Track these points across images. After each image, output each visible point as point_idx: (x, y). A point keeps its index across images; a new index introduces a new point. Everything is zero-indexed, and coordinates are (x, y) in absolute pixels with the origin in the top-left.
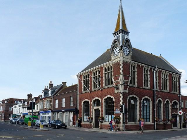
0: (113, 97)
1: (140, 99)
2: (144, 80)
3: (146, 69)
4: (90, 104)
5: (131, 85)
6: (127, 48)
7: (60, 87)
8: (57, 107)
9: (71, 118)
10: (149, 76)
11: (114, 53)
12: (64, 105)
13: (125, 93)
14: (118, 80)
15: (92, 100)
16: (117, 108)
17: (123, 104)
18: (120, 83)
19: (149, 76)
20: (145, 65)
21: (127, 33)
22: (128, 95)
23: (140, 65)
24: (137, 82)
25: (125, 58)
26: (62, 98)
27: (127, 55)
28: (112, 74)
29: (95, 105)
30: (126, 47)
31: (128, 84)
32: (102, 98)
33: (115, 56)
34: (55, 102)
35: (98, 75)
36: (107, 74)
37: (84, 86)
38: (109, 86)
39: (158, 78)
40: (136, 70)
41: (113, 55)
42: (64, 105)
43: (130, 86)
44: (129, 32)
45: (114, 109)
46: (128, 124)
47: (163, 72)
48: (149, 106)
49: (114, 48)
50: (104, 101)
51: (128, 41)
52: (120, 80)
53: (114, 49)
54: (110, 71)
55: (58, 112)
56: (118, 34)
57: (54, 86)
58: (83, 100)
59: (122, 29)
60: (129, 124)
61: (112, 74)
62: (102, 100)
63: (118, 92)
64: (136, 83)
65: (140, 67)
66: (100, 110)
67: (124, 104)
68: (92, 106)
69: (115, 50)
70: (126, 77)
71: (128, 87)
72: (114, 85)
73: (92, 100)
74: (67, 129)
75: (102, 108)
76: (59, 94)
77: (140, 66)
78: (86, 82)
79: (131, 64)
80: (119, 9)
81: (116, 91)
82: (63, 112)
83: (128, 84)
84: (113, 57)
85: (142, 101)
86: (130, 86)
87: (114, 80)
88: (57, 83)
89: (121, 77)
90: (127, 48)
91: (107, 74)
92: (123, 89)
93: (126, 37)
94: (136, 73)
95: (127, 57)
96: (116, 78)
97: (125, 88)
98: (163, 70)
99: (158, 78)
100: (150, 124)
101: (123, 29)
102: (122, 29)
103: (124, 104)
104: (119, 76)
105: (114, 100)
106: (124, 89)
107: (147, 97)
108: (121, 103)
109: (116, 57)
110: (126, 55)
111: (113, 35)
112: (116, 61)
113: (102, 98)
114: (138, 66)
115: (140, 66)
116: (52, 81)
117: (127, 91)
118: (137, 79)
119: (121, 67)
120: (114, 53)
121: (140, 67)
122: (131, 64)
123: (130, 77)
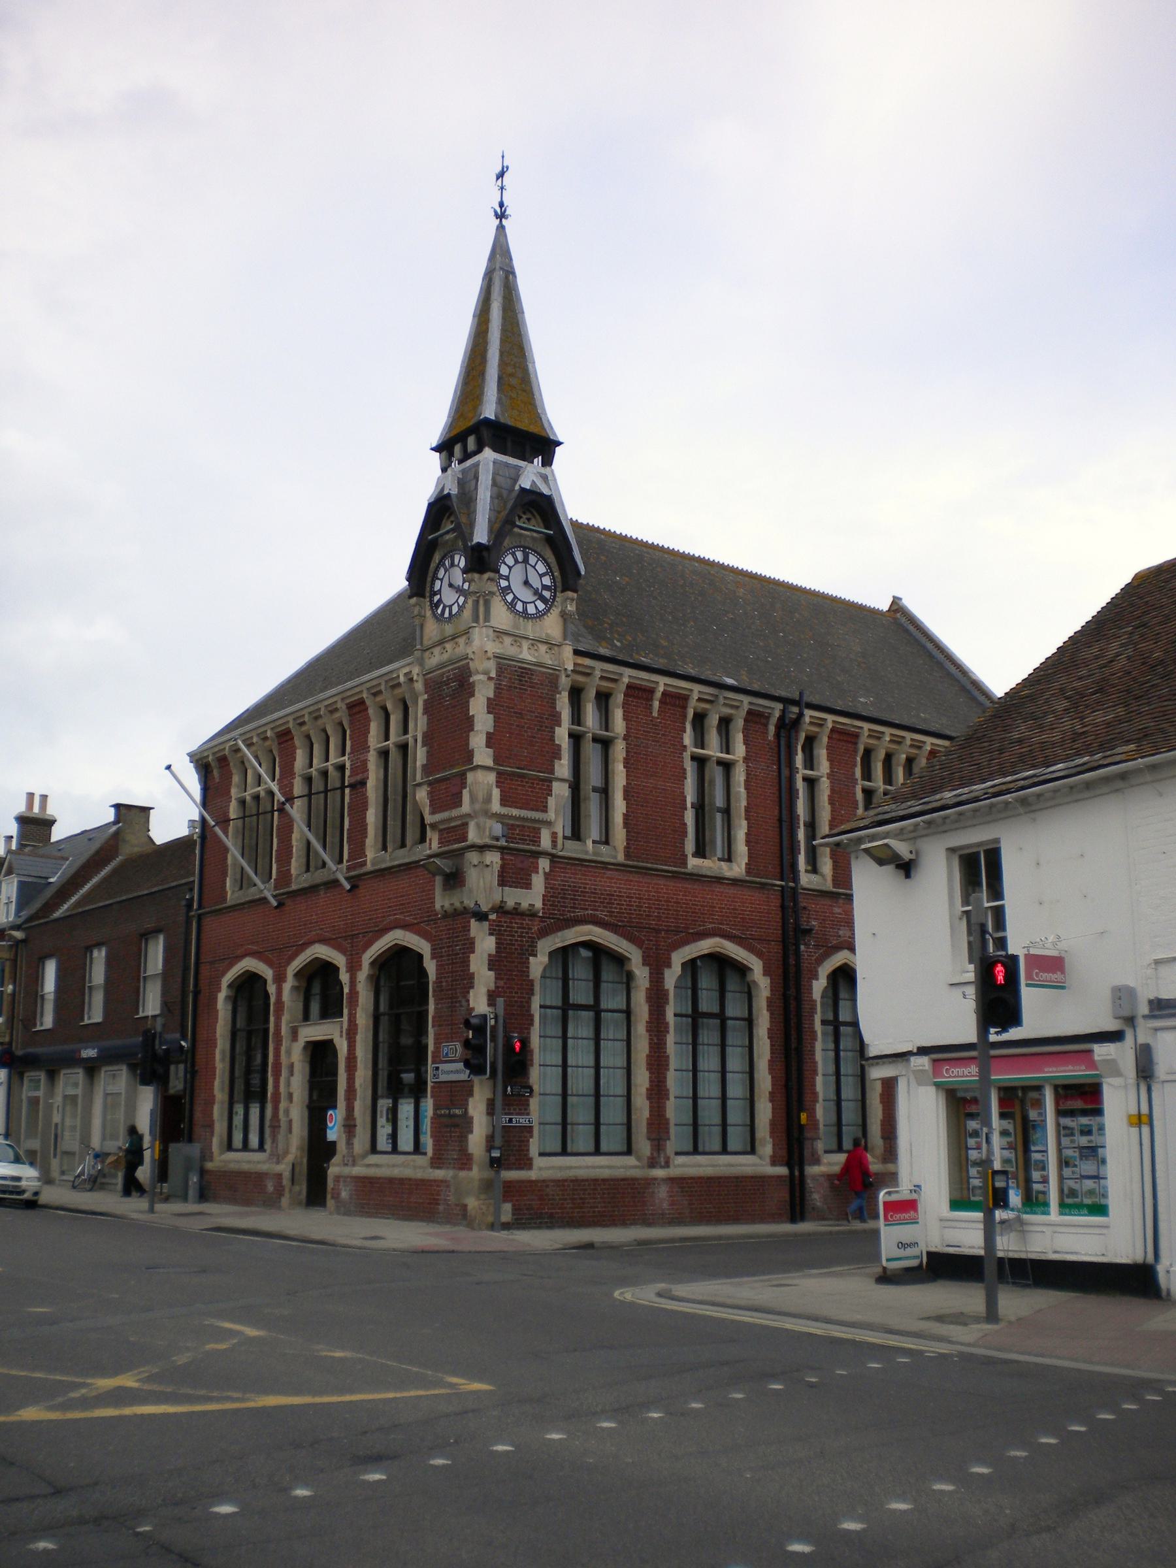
0: (423, 946)
1: (657, 964)
2: (700, 808)
3: (713, 720)
4: (273, 1000)
5: (572, 849)
6: (532, 559)
7: (96, 846)
8: (47, 1021)
9: (144, 1124)
10: (740, 775)
11: (436, 598)
12: (95, 1014)
13: (516, 912)
14: (455, 813)
15: (368, 956)
16: (450, 1039)
17: (491, 1002)
18: (473, 836)
19: (740, 775)
20: (697, 690)
21: (542, 446)
22: (544, 933)
23: (651, 691)
24: (626, 824)
25: (517, 638)
26: (89, 949)
27: (531, 609)
28: (420, 755)
29: (315, 1008)
30: (520, 556)
31: (536, 840)
32: (353, 948)
33: (439, 619)
34: (37, 979)
35: (334, 759)
36: (394, 755)
37: (308, 843)
38: (403, 857)
39: (824, 787)
40: (619, 724)
41: (429, 613)
42: (95, 1014)
43: (553, 858)
44: (561, 440)
45: (431, 1048)
46: (533, 1175)
47: (898, 741)
48: (750, 1021)
49: (437, 557)
50: (370, 977)
51: (542, 506)
52: (466, 807)
53: (433, 565)
54: (410, 736)
55: (53, 1068)
56: (466, 456)
57: (58, 833)
58: (231, 965)
59: (497, 423)
60: (546, 1175)
61: (420, 755)
62: (353, 967)
63: (457, 905)
64: (619, 835)
65: (656, 704)
66: (342, 1047)
67: (500, 1001)
68: (285, 1019)
69: (442, 571)
70: (523, 784)
71: (544, 864)
72: (435, 845)
73: (368, 956)
74: (45, 1206)
75: (353, 1036)
76: (78, 904)
77: (658, 695)
78: (334, 799)
79: (564, 682)
80: (489, 276)
81: (442, 901)
82: (91, 1069)
83: (545, 842)
84: (432, 630)
85: (672, 976)
86: (553, 858)
87: (433, 813)
88: (79, 814)
89: (483, 783)
90: (532, 559)
91: (394, 755)
92: (492, 877)
93: (530, 475)
94: (619, 750)
95: (529, 629)
96: (447, 793)
97: (514, 874)
98: (866, 726)
99: (824, 787)
100: (749, 1171)
101: (506, 420)
102: (497, 423)
103: (500, 1001)
104: (463, 775)
105: (430, 966)
106: (503, 882)
107: (717, 940)
108: (479, 1003)
109: (449, 629)
110: (525, 614)
111: (435, 460)
112: (445, 656)
113: (353, 948)
114: (634, 690)
115: (658, 695)
116: (44, 798)
117: (533, 896)
118: (626, 797)
119: (478, 707)
120: (436, 598)
121: (656, 704)
122: (564, 682)
123: (556, 786)
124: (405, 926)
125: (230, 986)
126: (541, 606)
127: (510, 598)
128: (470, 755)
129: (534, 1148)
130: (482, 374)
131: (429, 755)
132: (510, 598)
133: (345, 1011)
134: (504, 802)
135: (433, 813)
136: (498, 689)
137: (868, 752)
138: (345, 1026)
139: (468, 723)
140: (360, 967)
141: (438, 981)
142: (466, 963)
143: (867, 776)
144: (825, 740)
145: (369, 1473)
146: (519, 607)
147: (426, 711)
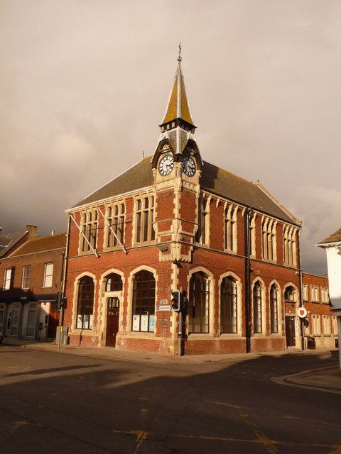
93: (189, 135)
105: (156, 277)
117: (188, 258)
119: (176, 201)
133: (123, 289)
134: (183, 229)
141: (159, 282)
142: (170, 276)
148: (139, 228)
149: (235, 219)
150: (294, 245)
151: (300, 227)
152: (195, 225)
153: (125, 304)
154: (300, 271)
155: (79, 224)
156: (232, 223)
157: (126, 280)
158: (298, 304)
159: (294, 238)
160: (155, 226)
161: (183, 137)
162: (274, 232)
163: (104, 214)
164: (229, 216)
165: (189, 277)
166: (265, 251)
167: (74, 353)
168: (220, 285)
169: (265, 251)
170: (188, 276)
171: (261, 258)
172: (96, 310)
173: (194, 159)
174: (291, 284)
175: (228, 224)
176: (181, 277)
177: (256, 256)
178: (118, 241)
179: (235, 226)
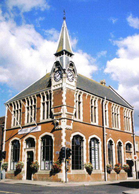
1: (87, 139)
4: (21, 144)
15: (40, 137)
27: (71, 80)
30: (69, 72)
64: (82, 117)
65: (86, 97)
87: (55, 112)
93: (70, 59)
105: (53, 138)
117: (71, 127)
119: (64, 95)
121: (86, 97)
124: (96, 135)
125: (11, 142)
126: (72, 80)
127: (68, 78)
128: (62, 103)
129: (130, 159)
130: (63, 41)
131: (54, 103)
132: (68, 78)
133: (36, 146)
134: (68, 111)
135: (55, 112)
136: (67, 93)
137: (92, 100)
138: (36, 148)
139: (62, 98)
140: (39, 139)
141: (55, 141)
142: (61, 137)
143: (92, 104)
144: (82, 96)
145: (126, 191)
146: (69, 80)
147: (53, 96)
148: (44, 111)
149: (97, 106)
150: (130, 119)
151: (133, 109)
152: (74, 109)
153: (107, 163)
154: (133, 134)
155: (12, 111)
156: (95, 108)
157: (37, 141)
158: (133, 153)
159: (130, 116)
160: (52, 110)
161: (67, 59)
162: (119, 113)
163: (25, 104)
164: (93, 104)
165: (71, 138)
166: (126, 126)
167: (9, 183)
168: (117, 146)
169: (126, 126)
170: (88, 140)
171: (124, 130)
172: (21, 158)
173: (73, 72)
174: (119, 140)
175: (93, 108)
176: (67, 138)
177: (121, 129)
178: (33, 119)
179: (97, 109)
